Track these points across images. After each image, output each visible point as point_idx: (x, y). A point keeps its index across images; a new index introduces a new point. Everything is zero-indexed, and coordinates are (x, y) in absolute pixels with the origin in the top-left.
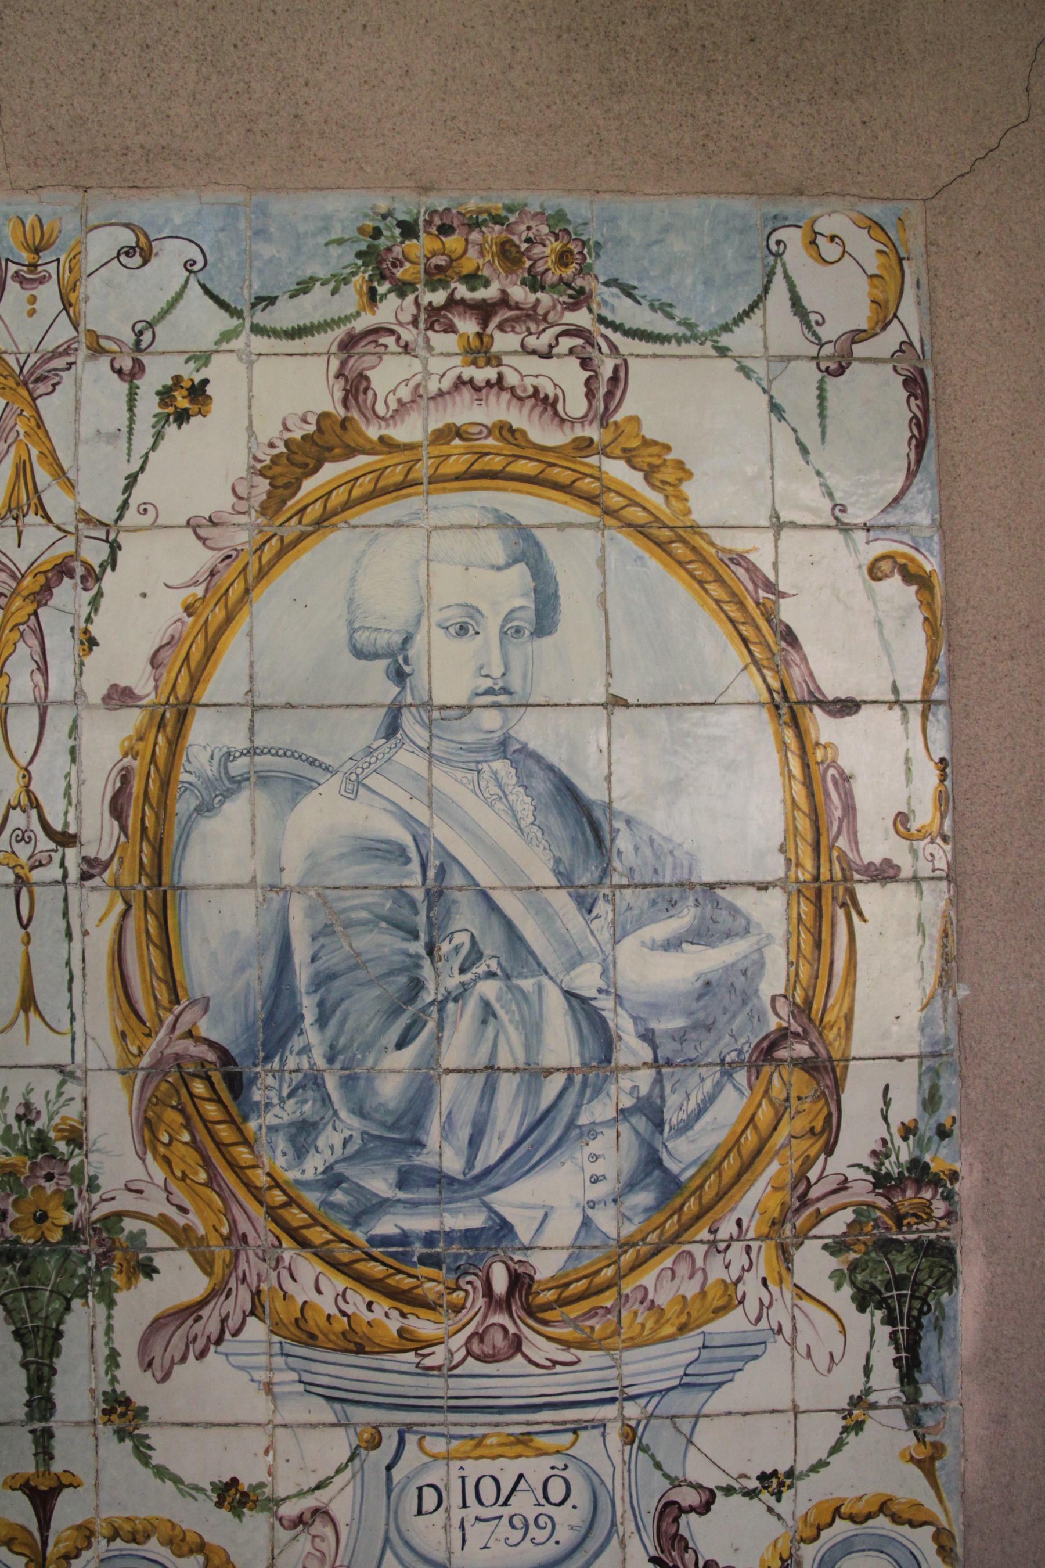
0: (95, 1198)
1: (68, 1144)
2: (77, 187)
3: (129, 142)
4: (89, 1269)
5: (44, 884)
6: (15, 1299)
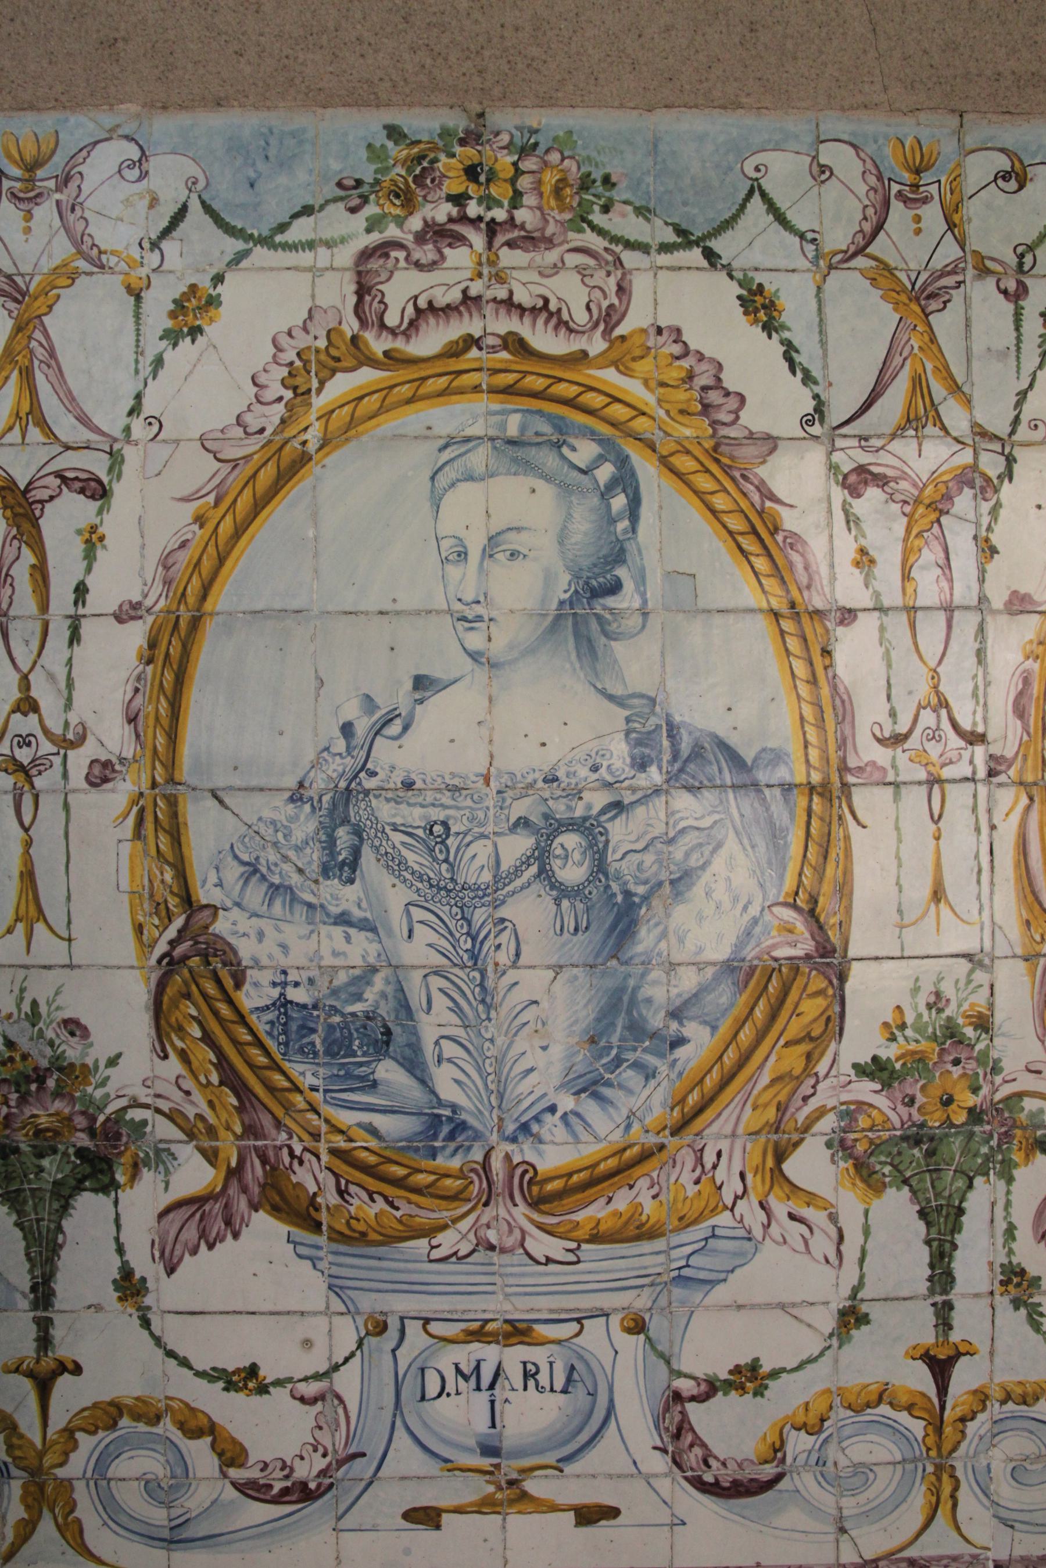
0: (998, 1080)
1: (975, 1029)
2: (953, 111)
3: (1000, 68)
4: (991, 1148)
5: (954, 781)
6: (920, 1181)
